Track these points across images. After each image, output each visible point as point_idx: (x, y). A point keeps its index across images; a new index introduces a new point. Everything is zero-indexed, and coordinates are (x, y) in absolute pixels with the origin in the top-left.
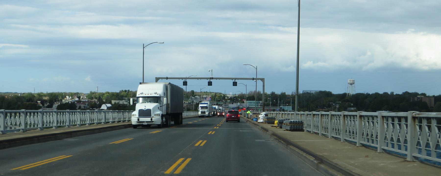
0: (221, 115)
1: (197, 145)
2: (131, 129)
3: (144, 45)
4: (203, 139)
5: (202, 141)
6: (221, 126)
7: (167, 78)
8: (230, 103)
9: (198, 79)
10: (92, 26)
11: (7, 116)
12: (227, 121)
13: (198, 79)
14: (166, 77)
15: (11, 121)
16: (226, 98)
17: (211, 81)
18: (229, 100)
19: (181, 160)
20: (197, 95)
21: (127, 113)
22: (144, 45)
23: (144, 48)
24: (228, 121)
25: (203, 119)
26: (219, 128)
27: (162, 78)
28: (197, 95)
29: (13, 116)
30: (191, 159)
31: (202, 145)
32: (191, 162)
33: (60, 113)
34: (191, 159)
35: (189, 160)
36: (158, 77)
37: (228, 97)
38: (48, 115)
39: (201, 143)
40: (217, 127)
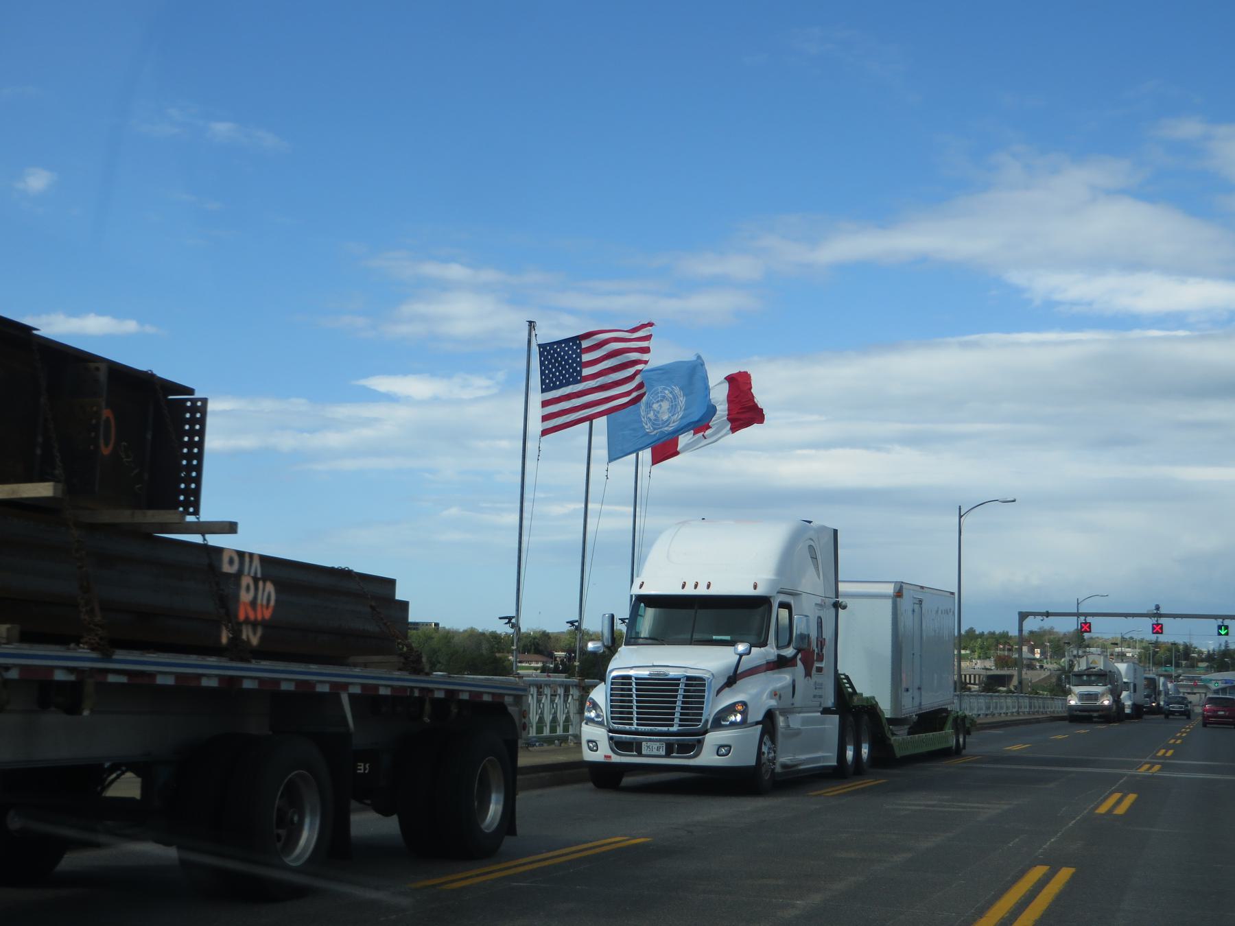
0: (1187, 714)
1: (1103, 809)
2: (582, 794)
3: (960, 509)
4: (1125, 790)
5: (1097, 811)
6: (1182, 743)
7: (1048, 614)
8: (1208, 670)
9: (1126, 615)
10: (813, 452)
11: (568, 695)
12: (1205, 725)
13: (1126, 615)
14: (1045, 611)
15: (540, 711)
16: (1196, 655)
17: (1159, 622)
18: (1202, 660)
19: (1038, 872)
20: (1095, 645)
21: (966, 697)
22: (960, 509)
23: (960, 517)
24: (1208, 725)
25: (1083, 730)
26: (1160, 770)
27: (1035, 614)
28: (1095, 645)
29: (532, 695)
30: (1072, 870)
31: (1120, 810)
32: (1073, 881)
33: (535, 690)
34: (1072, 870)
35: (1065, 874)
36: (1024, 610)
37: (1200, 653)
38: (544, 697)
39: (1117, 804)
40: (1177, 738)
